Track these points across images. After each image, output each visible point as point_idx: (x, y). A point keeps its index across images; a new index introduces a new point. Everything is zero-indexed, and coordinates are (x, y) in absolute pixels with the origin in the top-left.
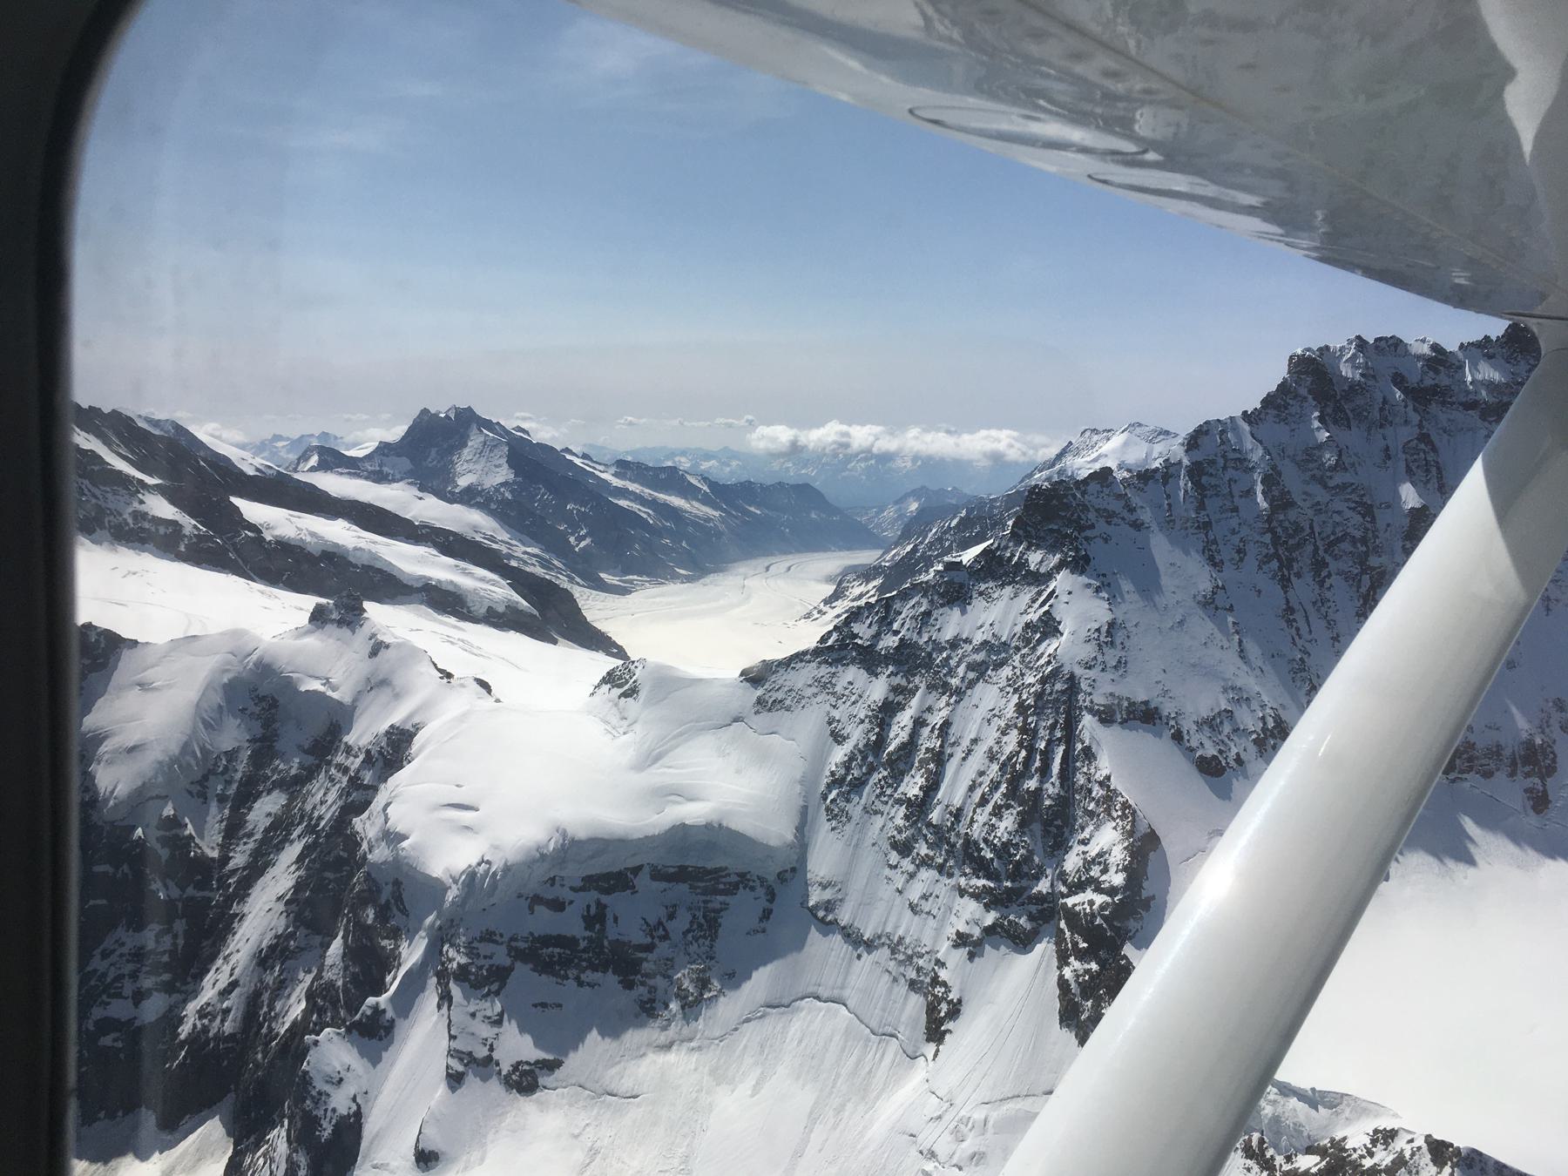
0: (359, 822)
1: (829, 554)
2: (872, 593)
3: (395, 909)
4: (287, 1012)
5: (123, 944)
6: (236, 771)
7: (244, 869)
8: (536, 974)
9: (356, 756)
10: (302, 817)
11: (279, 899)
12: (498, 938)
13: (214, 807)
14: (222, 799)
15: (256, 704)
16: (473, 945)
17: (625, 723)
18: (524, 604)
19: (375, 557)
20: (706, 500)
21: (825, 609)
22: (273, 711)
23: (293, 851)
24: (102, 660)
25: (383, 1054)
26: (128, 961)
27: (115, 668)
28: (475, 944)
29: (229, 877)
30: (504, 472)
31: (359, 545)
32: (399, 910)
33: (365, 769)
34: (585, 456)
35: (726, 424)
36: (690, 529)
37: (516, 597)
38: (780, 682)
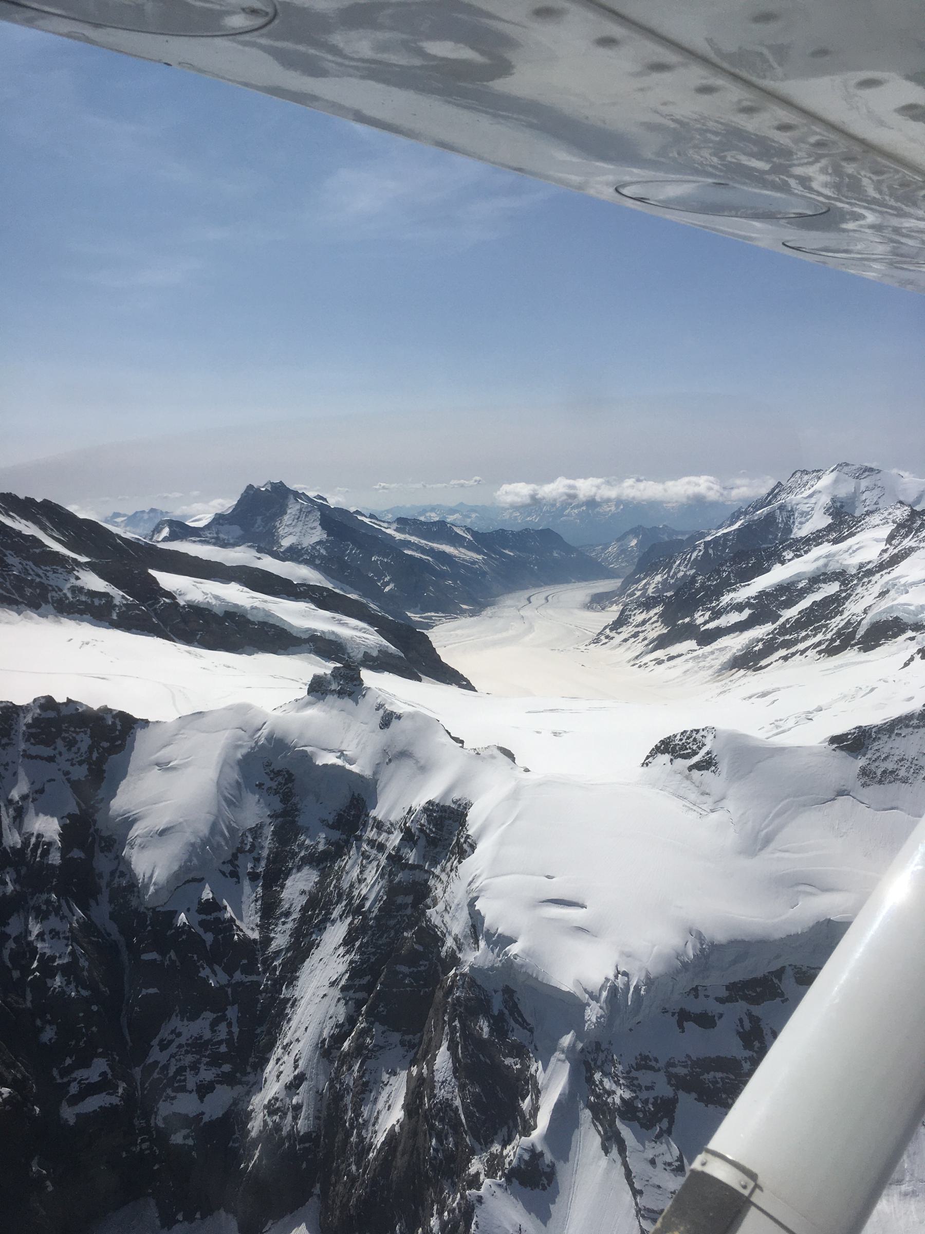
0: (434, 914)
1: (570, 586)
2: (655, 619)
3: (512, 1023)
4: (377, 1118)
5: (179, 1035)
6: (262, 848)
7: (288, 950)
8: (702, 1105)
9: (390, 832)
10: (340, 896)
11: (332, 984)
12: (653, 1063)
13: (246, 884)
14: (254, 877)
15: (272, 779)
16: (631, 1075)
17: (710, 800)
18: (392, 648)
19: (268, 614)
20: (470, 547)
21: (611, 635)
22: (290, 785)
23: (336, 933)
24: (119, 742)
25: (551, 1206)
26: (187, 1052)
27: (132, 748)
28: (634, 1074)
29: (274, 959)
30: (318, 533)
31: (255, 605)
32: (516, 1021)
33: (405, 847)
34: (372, 516)
35: (458, 484)
36: (462, 571)
37: (385, 643)
38: (886, 750)
